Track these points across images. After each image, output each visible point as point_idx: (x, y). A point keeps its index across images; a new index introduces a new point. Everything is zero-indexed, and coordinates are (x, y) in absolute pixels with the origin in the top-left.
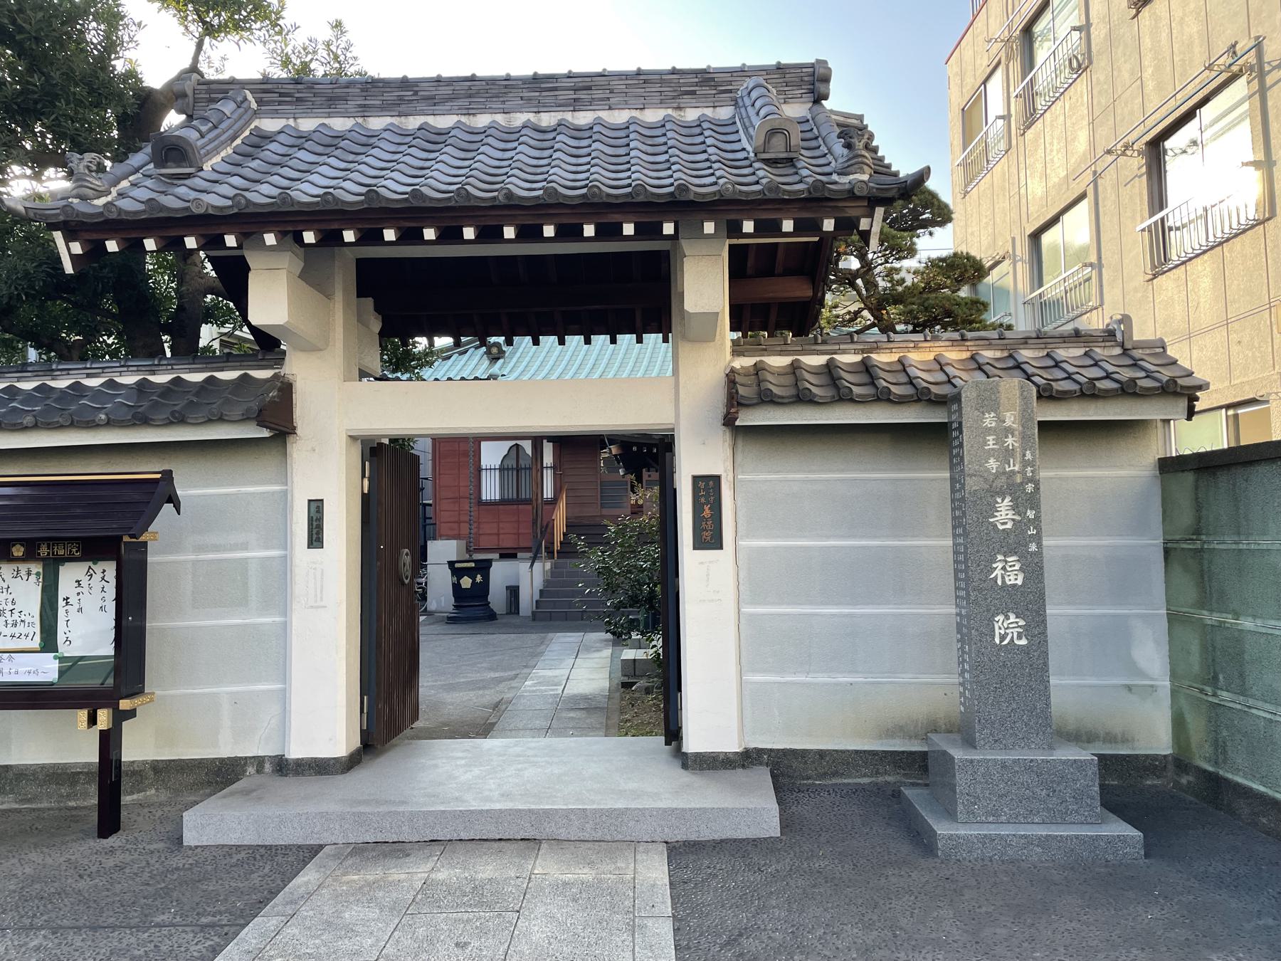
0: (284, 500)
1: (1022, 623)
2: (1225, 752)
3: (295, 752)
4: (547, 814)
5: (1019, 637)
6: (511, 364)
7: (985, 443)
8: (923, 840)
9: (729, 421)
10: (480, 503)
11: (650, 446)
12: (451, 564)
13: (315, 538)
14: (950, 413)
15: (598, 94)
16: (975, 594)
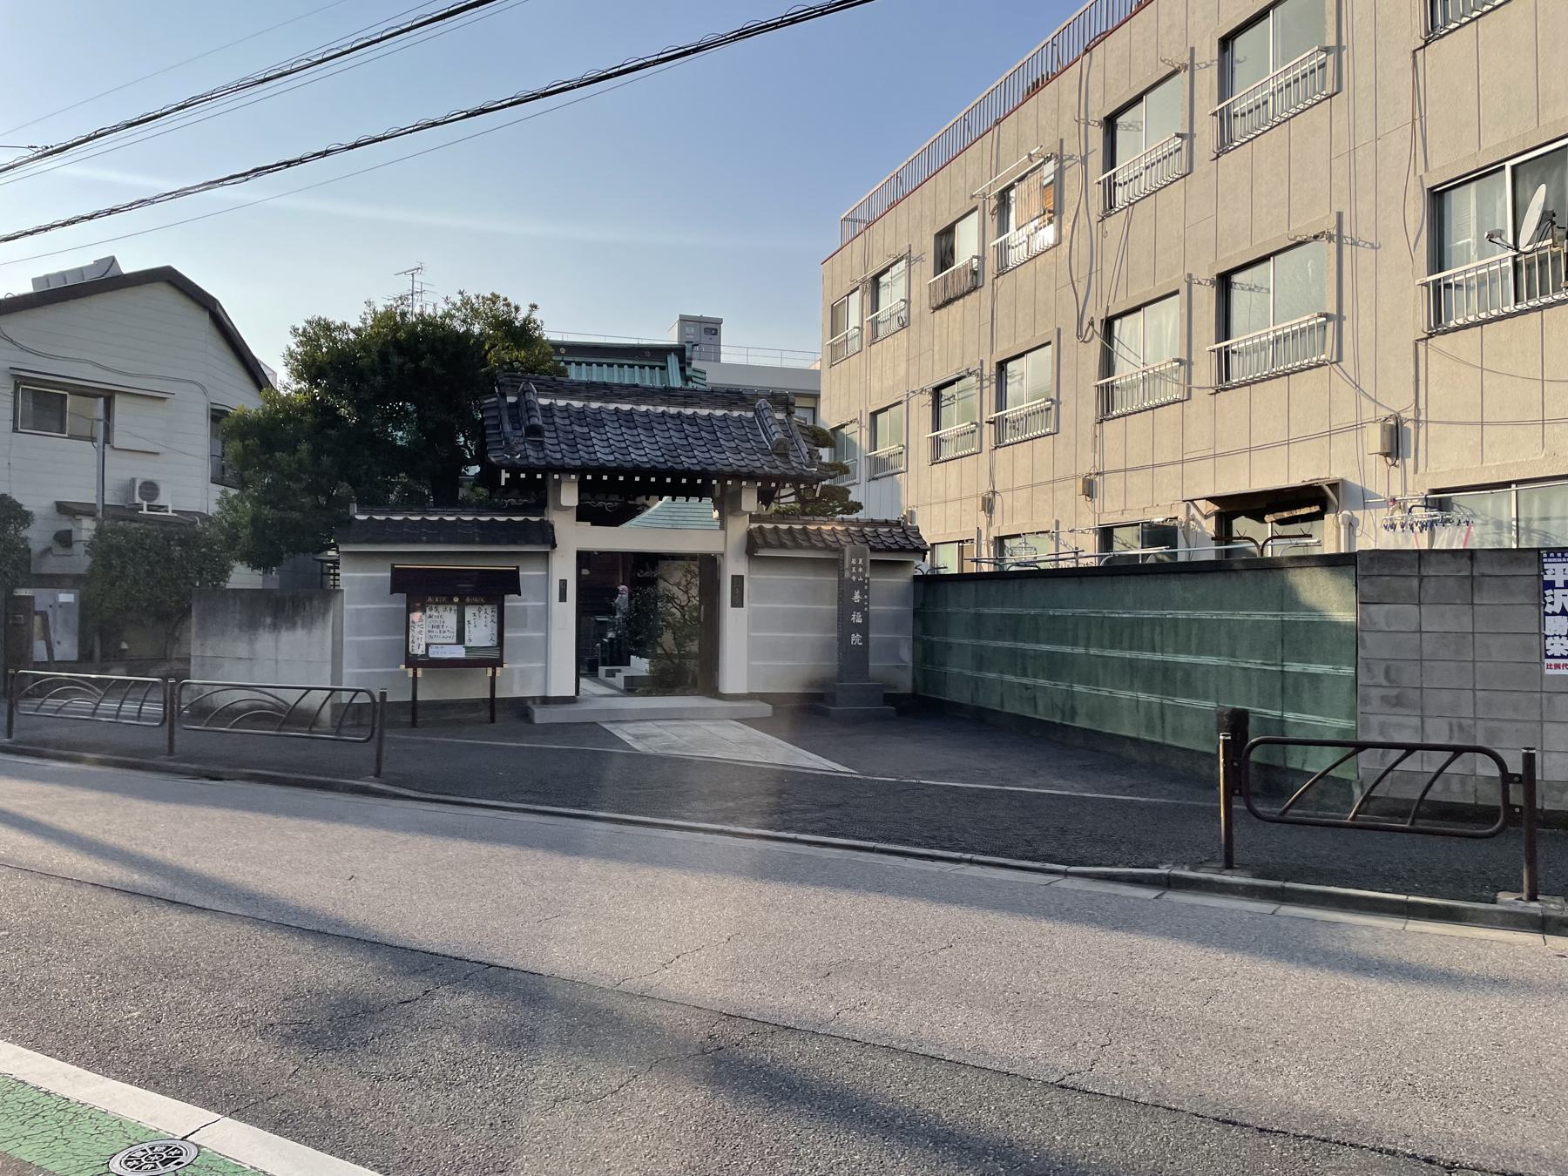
0: (547, 577)
3: (553, 693)
13: (563, 598)
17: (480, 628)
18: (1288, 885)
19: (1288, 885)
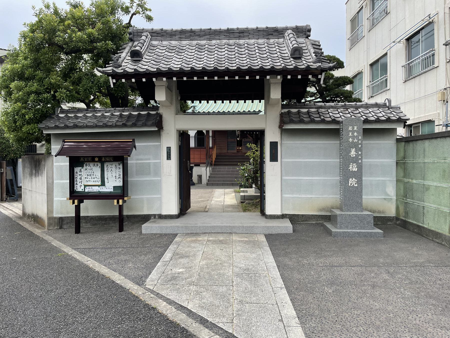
1: (356, 180)
2: (408, 215)
3: (164, 213)
4: (234, 227)
5: (355, 184)
7: (349, 134)
8: (329, 232)
9: (280, 127)
13: (169, 157)
14: (340, 126)
15: (245, 34)
16: (346, 174)
17: (113, 179)
18: (211, 139)
19: (211, 139)
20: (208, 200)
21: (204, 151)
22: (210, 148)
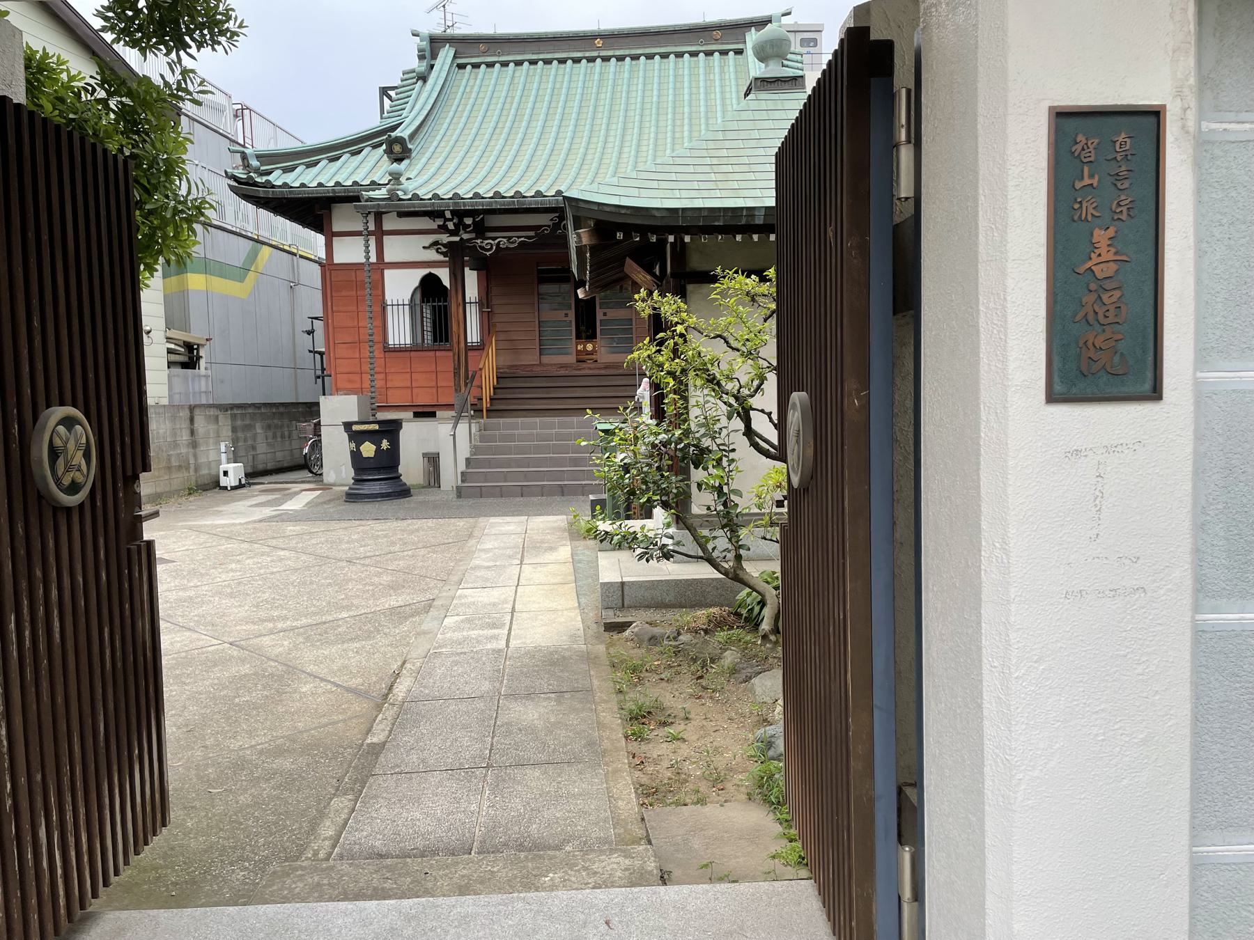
6: (419, 166)
10: (387, 350)
11: (644, 230)
12: (348, 426)
20: (429, 605)
21: (445, 360)
22: (469, 348)
